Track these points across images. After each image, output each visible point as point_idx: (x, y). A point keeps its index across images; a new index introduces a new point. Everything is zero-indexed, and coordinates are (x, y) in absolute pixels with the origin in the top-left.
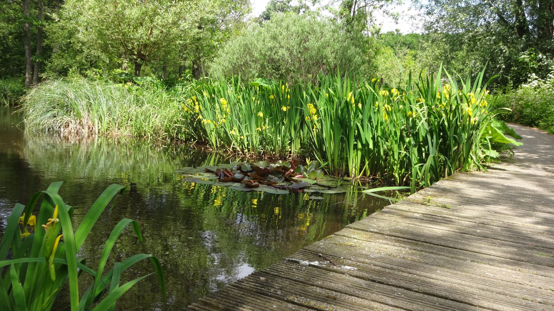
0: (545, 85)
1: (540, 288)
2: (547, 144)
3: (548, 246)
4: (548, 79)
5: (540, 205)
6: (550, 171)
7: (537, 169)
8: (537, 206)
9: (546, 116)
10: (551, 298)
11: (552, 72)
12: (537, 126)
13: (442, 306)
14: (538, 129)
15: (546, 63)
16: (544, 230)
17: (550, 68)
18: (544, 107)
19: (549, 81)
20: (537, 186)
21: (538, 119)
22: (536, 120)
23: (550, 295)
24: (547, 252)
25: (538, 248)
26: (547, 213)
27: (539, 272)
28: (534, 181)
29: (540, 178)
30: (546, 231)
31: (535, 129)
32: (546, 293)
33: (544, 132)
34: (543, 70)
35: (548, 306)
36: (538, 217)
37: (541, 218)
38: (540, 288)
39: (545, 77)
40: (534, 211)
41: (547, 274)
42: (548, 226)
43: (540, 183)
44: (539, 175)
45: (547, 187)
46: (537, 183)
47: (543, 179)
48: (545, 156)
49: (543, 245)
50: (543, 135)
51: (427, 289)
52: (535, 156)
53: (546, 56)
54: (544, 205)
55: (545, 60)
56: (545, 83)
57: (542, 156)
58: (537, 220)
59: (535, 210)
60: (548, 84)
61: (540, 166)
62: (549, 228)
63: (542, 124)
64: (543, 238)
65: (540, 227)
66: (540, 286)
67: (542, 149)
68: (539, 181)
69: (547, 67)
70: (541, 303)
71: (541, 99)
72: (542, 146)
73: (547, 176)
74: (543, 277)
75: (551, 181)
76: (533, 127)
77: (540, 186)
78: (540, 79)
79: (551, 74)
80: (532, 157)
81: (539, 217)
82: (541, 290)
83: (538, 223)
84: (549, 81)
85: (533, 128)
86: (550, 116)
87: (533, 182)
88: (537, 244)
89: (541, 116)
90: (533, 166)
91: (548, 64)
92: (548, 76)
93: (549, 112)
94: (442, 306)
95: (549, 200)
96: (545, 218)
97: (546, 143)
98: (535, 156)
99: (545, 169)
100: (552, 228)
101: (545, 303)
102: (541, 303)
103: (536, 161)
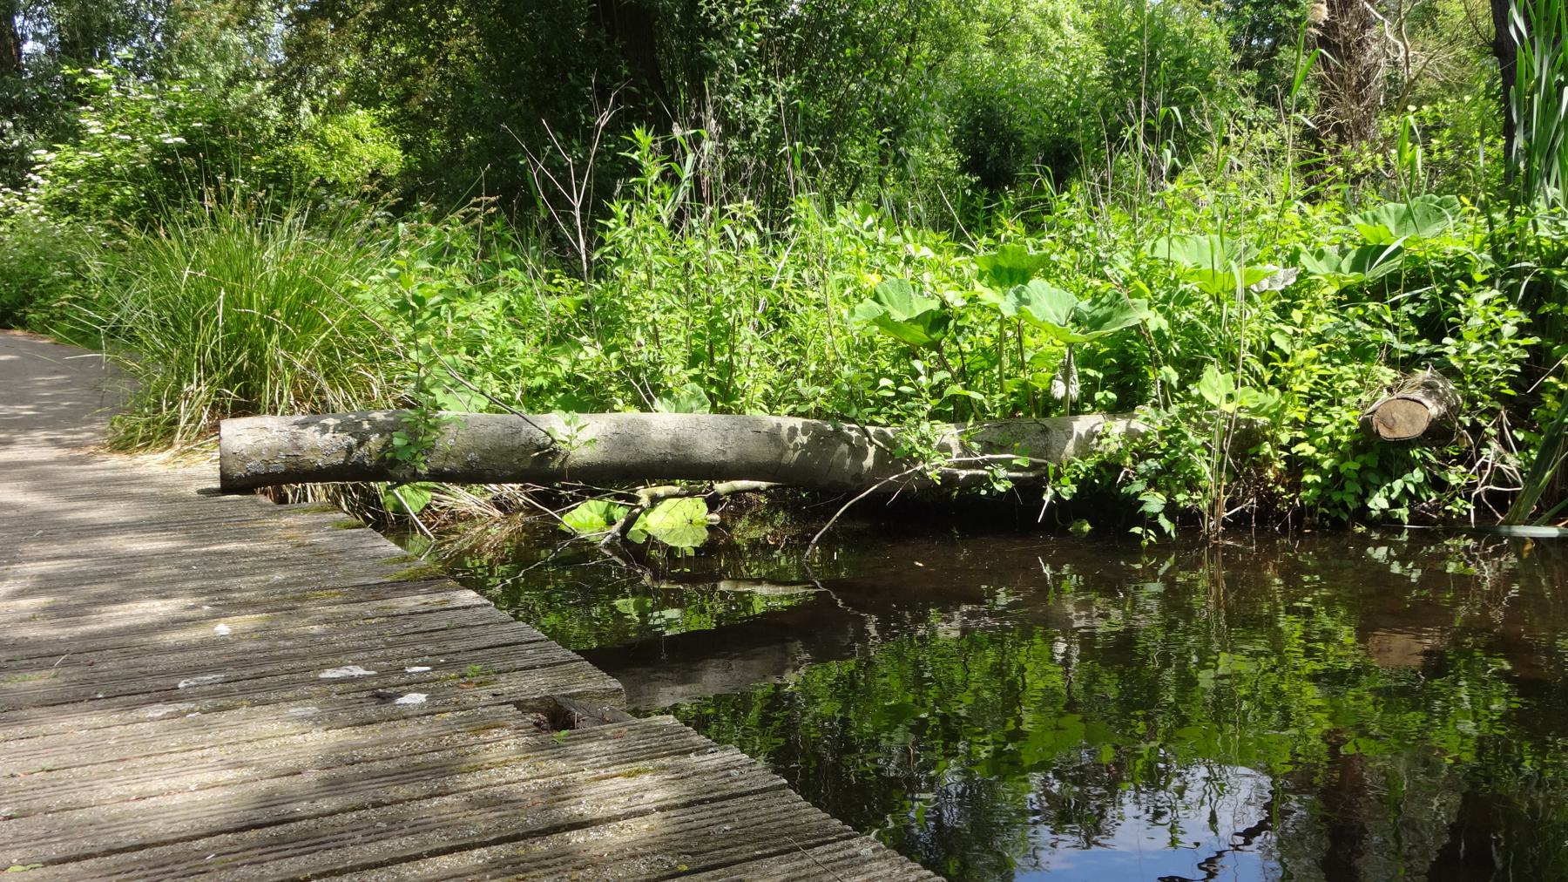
0: (26, 206)
1: (13, 776)
2: (56, 373)
3: (44, 652)
4: (33, 190)
5: (32, 542)
6: (66, 446)
7: (34, 443)
8: (22, 547)
9: (42, 295)
10: (41, 794)
11: (37, 167)
12: (23, 323)
13: (308, 842)
14: (26, 333)
15: (16, 143)
16: (36, 609)
17: (32, 158)
18: (32, 269)
19: (35, 195)
20: (26, 491)
21: (22, 304)
22: (17, 308)
23: (41, 785)
24: (41, 668)
25: (13, 664)
26: (49, 559)
27: (11, 732)
28: (16, 480)
29: (38, 468)
30: (44, 610)
31: (19, 333)
32: (28, 784)
33: (43, 338)
34: (12, 162)
35: (32, 820)
36: (21, 577)
37: (31, 577)
38: (13, 776)
39: (24, 183)
40: (13, 563)
41: (34, 729)
42: (48, 594)
43: (35, 483)
44: (35, 459)
45: (56, 490)
46: (27, 484)
47: (45, 471)
48: (57, 405)
49: (30, 652)
50: (43, 349)
51: (105, 841)
52: (25, 410)
53: (13, 121)
54: (42, 539)
55: (12, 133)
56: (24, 199)
57: (47, 408)
58: (17, 588)
59: (14, 560)
60: (32, 204)
61: (40, 435)
62: (51, 599)
63: (33, 316)
64: (31, 632)
65: (25, 603)
66: (11, 770)
67: (43, 387)
68: (34, 477)
69: (22, 154)
70: (10, 818)
71: (18, 247)
72: (42, 380)
73: (59, 461)
74: (22, 743)
75: (68, 471)
76: (11, 328)
77: (36, 489)
78: (8, 190)
79: (35, 173)
80: (16, 415)
81: (24, 577)
82: (13, 781)
83: (21, 594)
84: (35, 195)
85: (11, 332)
86: (51, 293)
87: (15, 484)
88: (11, 655)
89: (27, 295)
90: (21, 438)
91: (22, 144)
92: (30, 180)
93: (47, 281)
94: (308, 842)
95: (59, 523)
96: (40, 576)
97: (53, 368)
98: (25, 410)
99: (57, 443)
100: (58, 598)
101: (24, 814)
102: (10, 818)
103: (27, 425)
